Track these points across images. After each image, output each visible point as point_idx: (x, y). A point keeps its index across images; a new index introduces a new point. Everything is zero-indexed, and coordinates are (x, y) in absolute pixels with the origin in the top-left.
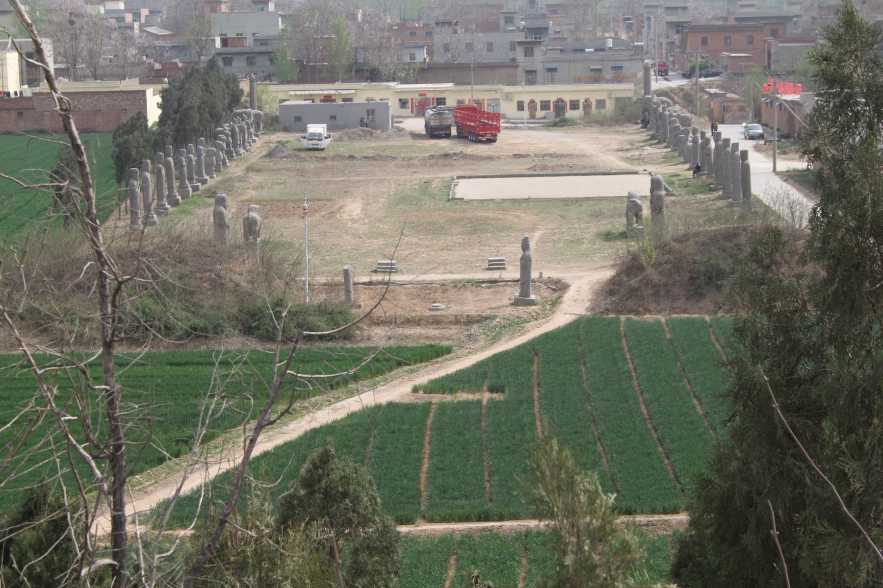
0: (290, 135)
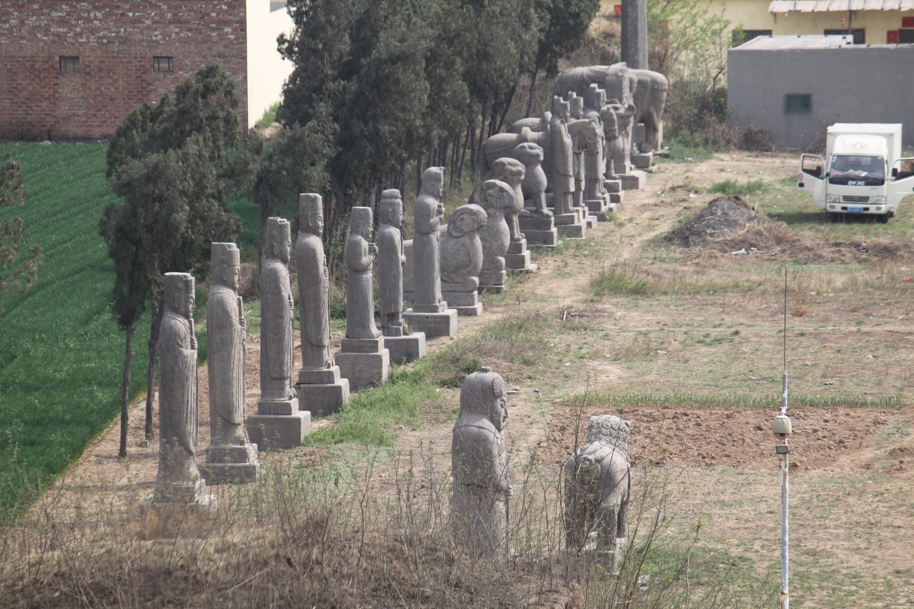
0: (767, 161)
